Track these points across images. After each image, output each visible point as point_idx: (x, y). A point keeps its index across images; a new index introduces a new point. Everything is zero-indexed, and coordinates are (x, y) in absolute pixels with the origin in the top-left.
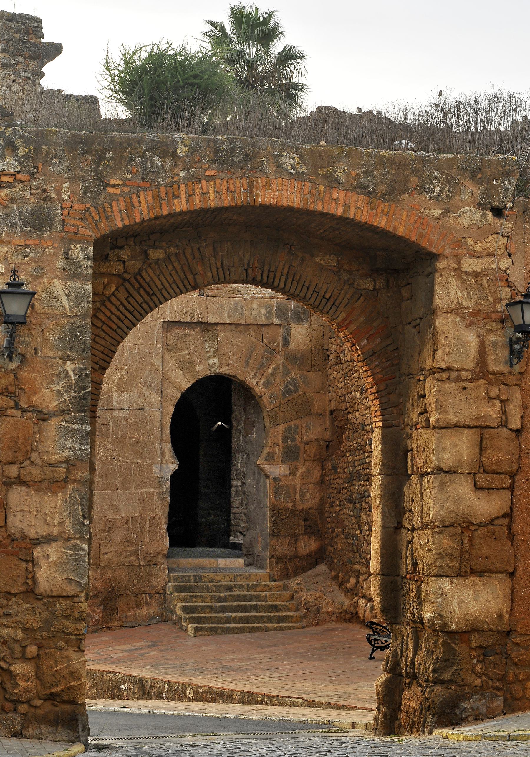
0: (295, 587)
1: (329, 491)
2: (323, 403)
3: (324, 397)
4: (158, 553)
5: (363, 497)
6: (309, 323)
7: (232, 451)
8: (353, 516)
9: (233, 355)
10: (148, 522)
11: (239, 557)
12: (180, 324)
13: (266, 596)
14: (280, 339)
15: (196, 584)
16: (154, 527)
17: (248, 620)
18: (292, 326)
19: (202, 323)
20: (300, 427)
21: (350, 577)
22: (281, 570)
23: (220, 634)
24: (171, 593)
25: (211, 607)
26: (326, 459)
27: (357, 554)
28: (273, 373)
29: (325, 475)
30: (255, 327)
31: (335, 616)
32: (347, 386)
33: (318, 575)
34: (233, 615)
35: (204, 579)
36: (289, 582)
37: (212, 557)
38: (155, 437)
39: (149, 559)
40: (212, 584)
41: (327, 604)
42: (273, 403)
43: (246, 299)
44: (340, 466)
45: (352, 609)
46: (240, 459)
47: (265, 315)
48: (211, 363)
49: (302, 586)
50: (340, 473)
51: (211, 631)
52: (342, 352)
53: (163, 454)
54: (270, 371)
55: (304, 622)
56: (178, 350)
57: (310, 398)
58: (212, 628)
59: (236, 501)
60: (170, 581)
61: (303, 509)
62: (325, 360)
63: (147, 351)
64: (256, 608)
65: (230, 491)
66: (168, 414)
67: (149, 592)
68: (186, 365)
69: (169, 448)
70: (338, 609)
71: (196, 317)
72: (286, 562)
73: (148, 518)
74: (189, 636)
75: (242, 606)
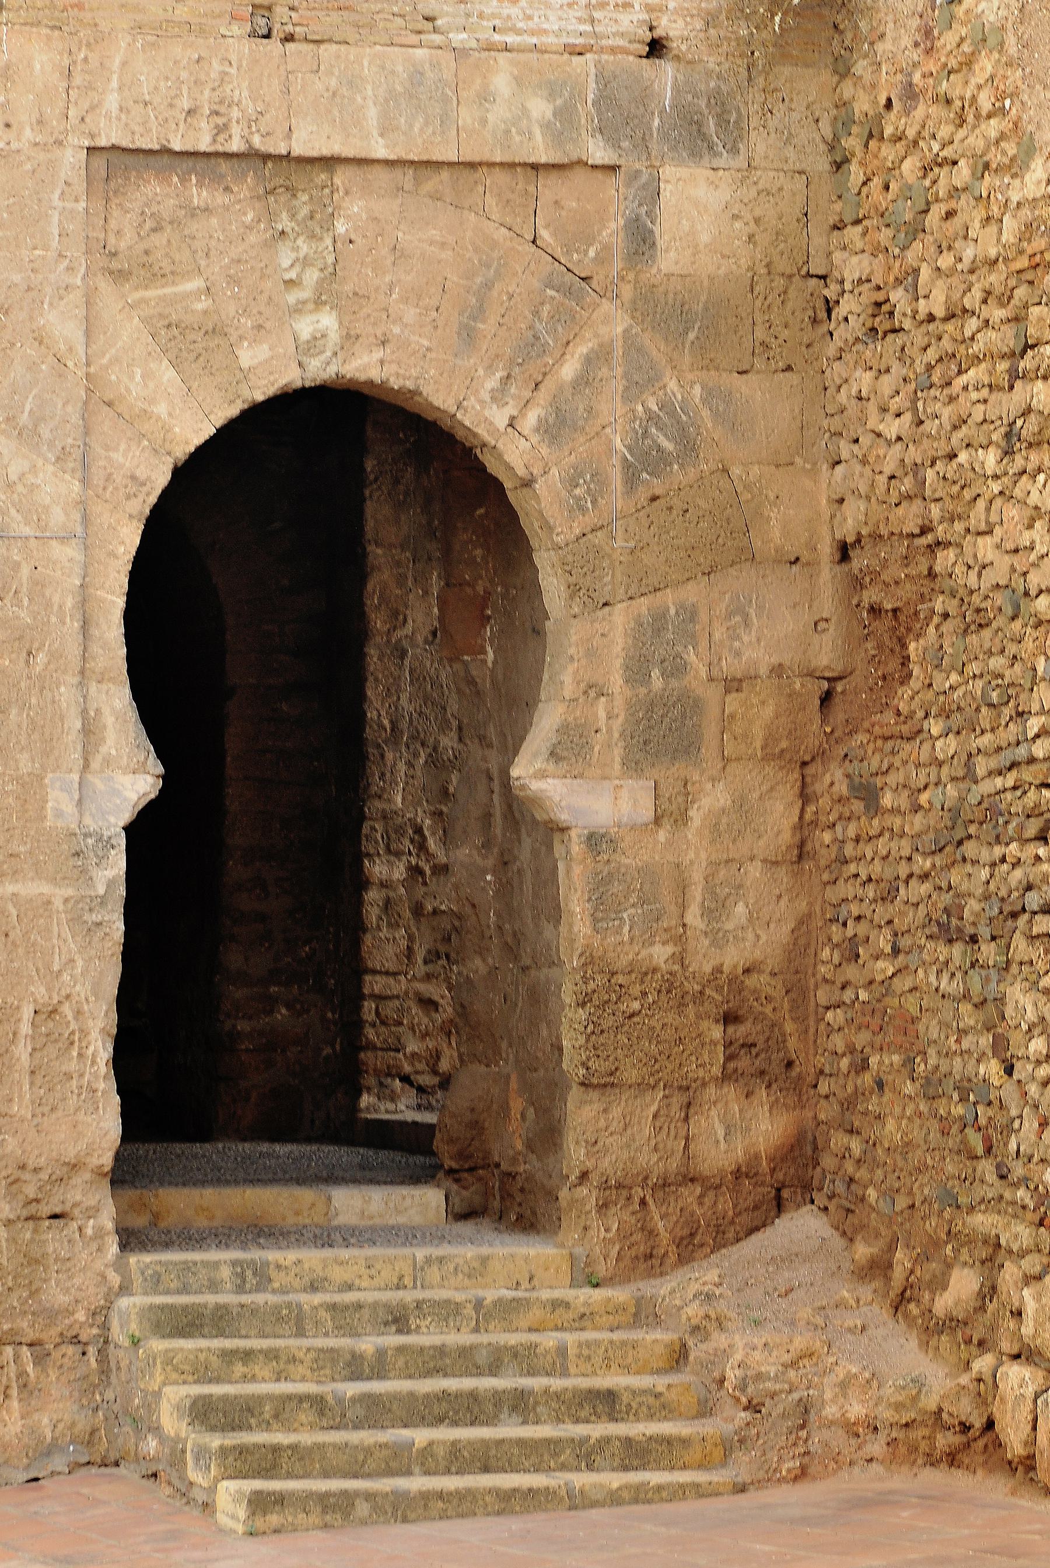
0: (694, 1311)
1: (833, 894)
2: (802, 510)
3: (808, 483)
4: (74, 1167)
5: (1014, 915)
6: (741, 161)
7: (369, 733)
8: (966, 996)
9: (405, 300)
10: (25, 1028)
11: (415, 1179)
12: (166, 159)
13: (562, 1351)
14: (612, 230)
15: (246, 1299)
16: (52, 1050)
17: (485, 1458)
18: (668, 171)
19: (266, 157)
20: (703, 616)
21: (949, 1266)
22: (623, 1235)
23: (364, 1522)
24: (136, 1342)
25: (318, 1403)
26: (820, 755)
27: (987, 1168)
28: (583, 381)
29: (814, 823)
30: (501, 177)
31: (882, 1437)
32: (931, 426)
33: (788, 1259)
34: (421, 1436)
35: (279, 1279)
36: (663, 1288)
37: (301, 1181)
38: (55, 656)
39: (31, 1191)
40: (317, 1299)
41: (843, 1386)
42: (583, 510)
43: (460, 53)
44: (892, 779)
45: (966, 1409)
46: (402, 767)
47: (546, 126)
48: (305, 334)
49: (722, 1306)
50: (894, 811)
51: (325, 1511)
52: (898, 281)
53: (90, 732)
54: (568, 371)
55: (742, 1466)
56: (156, 277)
57: (747, 487)
58: (328, 1494)
59: (384, 945)
60: (125, 1289)
61: (718, 970)
62: (815, 321)
63: (17, 278)
64: (521, 1404)
65: (359, 903)
66: (113, 555)
67: (31, 1335)
68: (191, 341)
69: (118, 704)
70: (898, 1407)
71: (236, 130)
72: (643, 1202)
73: (27, 1012)
74: (221, 1530)
75: (458, 1395)
